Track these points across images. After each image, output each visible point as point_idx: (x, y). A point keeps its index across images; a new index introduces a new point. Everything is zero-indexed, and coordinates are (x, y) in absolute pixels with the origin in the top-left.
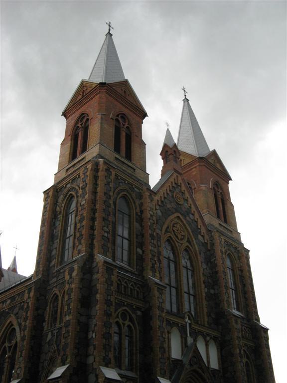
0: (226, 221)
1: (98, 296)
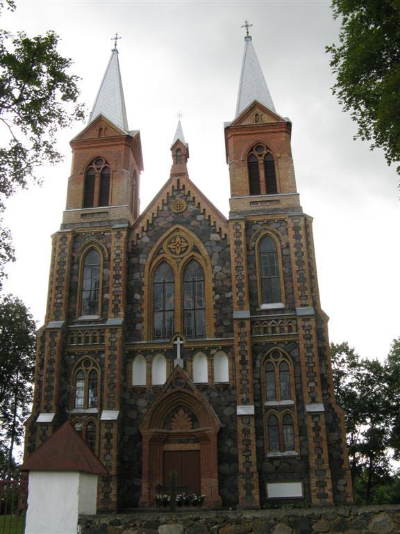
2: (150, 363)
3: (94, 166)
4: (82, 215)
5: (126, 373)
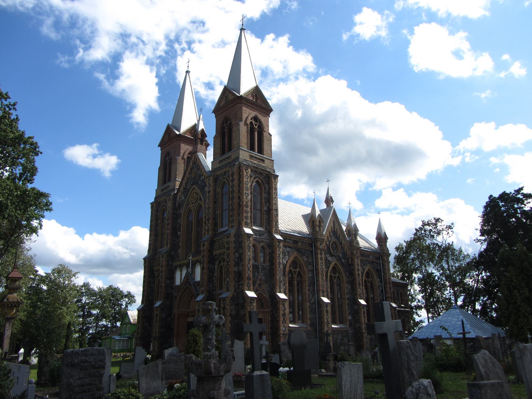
0: (261, 151)
1: (180, 244)
2: (181, 271)
3: (225, 125)
4: (162, 190)
5: (172, 278)
